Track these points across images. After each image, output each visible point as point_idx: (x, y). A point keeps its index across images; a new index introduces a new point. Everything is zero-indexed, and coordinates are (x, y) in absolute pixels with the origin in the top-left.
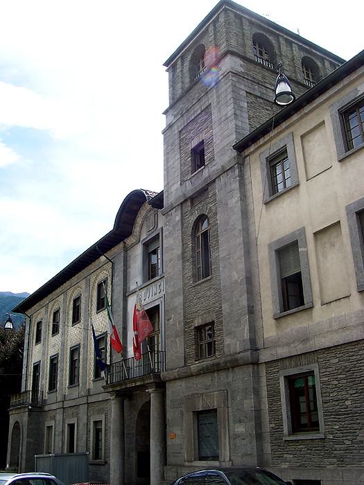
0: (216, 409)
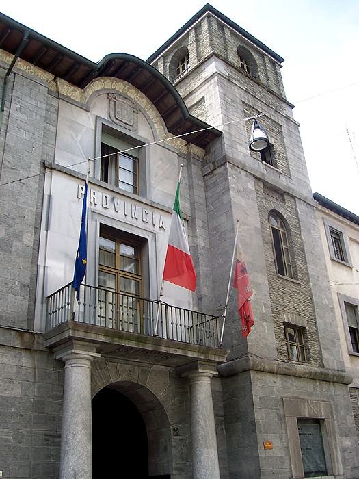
0: (324, 419)
